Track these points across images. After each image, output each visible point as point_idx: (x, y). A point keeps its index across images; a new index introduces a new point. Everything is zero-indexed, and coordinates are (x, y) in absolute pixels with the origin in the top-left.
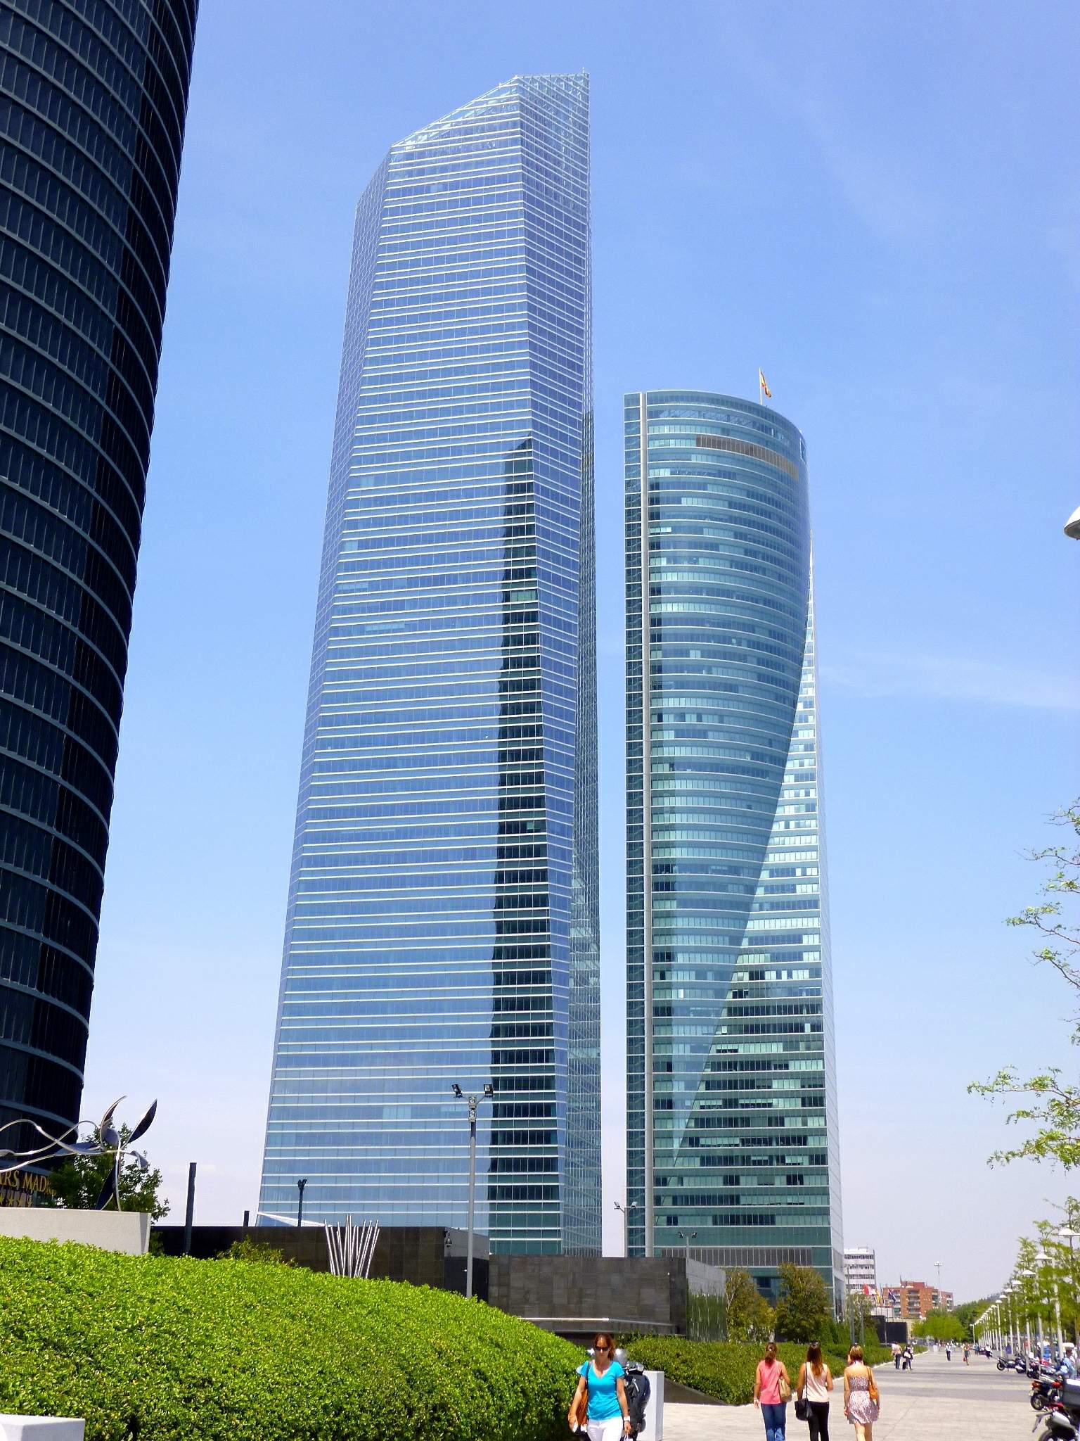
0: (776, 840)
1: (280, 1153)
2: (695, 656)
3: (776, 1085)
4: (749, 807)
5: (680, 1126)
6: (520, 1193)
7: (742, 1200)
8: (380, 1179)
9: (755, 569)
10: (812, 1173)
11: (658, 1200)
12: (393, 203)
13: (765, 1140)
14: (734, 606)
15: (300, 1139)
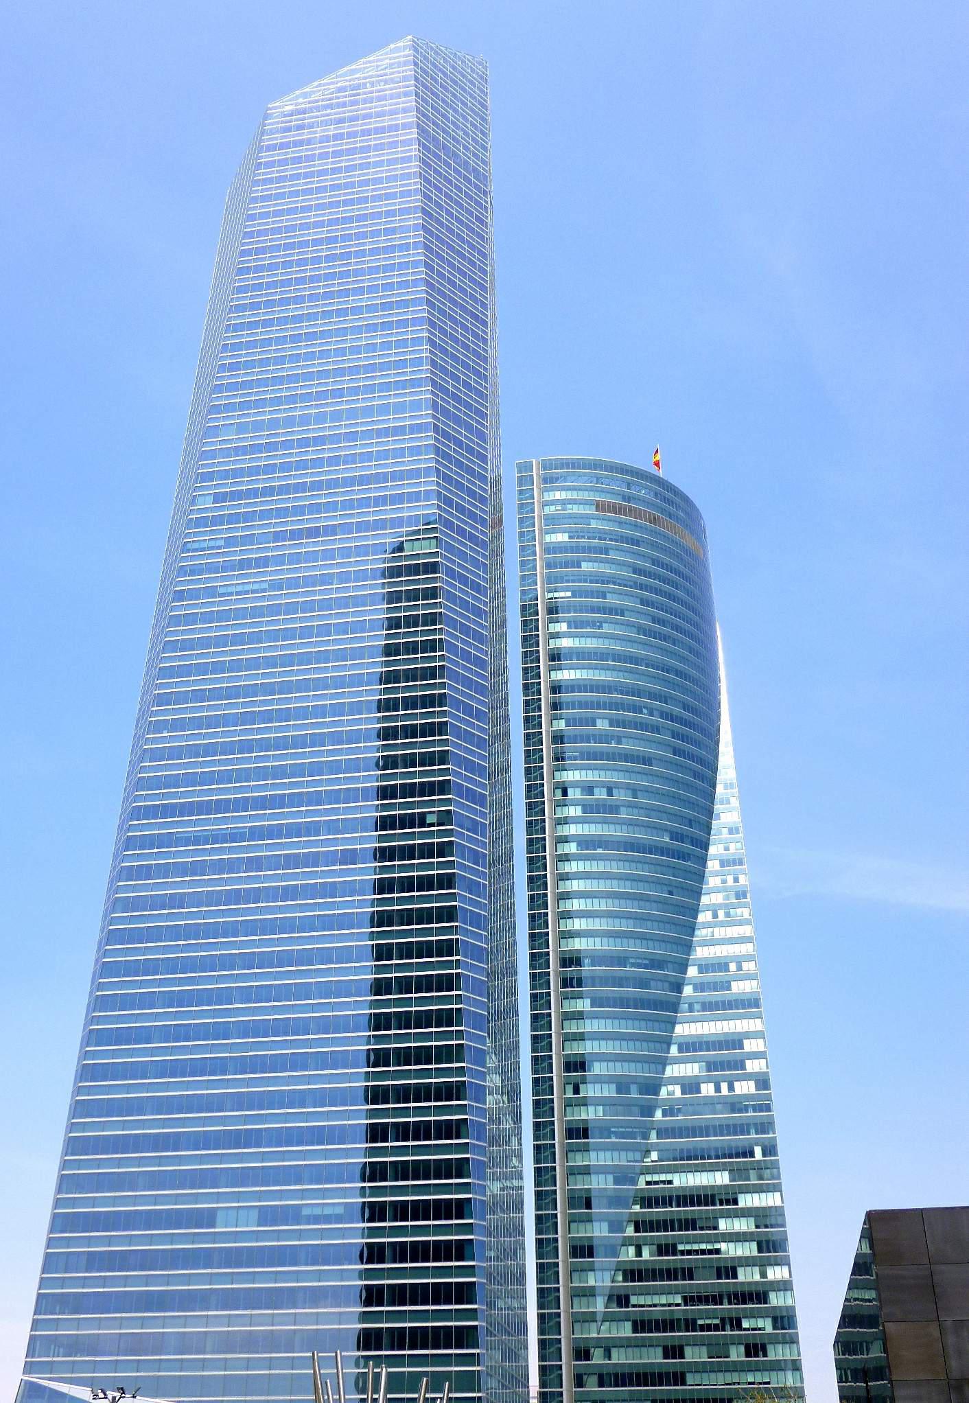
0: (704, 931)
1: (63, 1282)
2: (602, 725)
3: (724, 1225)
4: (671, 893)
5: (601, 1279)
6: (418, 1338)
7: (690, 1378)
8: (207, 1320)
9: (664, 638)
10: (775, 1340)
11: (579, 1381)
12: (265, 157)
13: (714, 1297)
14: (643, 674)
15: (94, 1261)
